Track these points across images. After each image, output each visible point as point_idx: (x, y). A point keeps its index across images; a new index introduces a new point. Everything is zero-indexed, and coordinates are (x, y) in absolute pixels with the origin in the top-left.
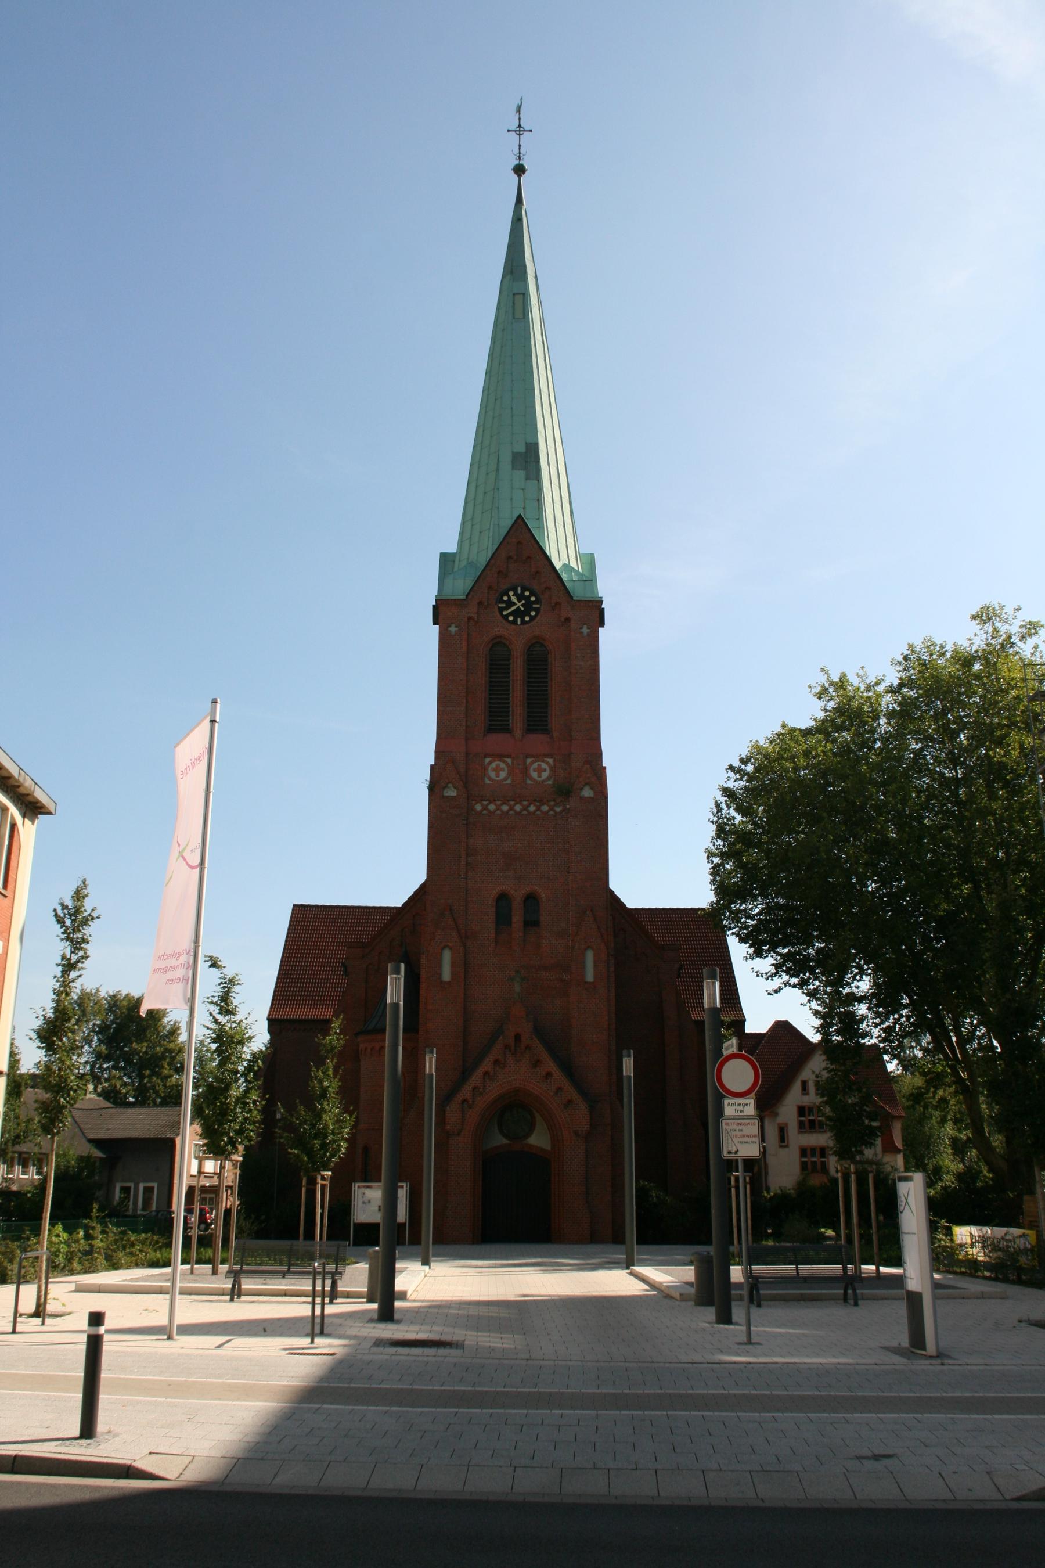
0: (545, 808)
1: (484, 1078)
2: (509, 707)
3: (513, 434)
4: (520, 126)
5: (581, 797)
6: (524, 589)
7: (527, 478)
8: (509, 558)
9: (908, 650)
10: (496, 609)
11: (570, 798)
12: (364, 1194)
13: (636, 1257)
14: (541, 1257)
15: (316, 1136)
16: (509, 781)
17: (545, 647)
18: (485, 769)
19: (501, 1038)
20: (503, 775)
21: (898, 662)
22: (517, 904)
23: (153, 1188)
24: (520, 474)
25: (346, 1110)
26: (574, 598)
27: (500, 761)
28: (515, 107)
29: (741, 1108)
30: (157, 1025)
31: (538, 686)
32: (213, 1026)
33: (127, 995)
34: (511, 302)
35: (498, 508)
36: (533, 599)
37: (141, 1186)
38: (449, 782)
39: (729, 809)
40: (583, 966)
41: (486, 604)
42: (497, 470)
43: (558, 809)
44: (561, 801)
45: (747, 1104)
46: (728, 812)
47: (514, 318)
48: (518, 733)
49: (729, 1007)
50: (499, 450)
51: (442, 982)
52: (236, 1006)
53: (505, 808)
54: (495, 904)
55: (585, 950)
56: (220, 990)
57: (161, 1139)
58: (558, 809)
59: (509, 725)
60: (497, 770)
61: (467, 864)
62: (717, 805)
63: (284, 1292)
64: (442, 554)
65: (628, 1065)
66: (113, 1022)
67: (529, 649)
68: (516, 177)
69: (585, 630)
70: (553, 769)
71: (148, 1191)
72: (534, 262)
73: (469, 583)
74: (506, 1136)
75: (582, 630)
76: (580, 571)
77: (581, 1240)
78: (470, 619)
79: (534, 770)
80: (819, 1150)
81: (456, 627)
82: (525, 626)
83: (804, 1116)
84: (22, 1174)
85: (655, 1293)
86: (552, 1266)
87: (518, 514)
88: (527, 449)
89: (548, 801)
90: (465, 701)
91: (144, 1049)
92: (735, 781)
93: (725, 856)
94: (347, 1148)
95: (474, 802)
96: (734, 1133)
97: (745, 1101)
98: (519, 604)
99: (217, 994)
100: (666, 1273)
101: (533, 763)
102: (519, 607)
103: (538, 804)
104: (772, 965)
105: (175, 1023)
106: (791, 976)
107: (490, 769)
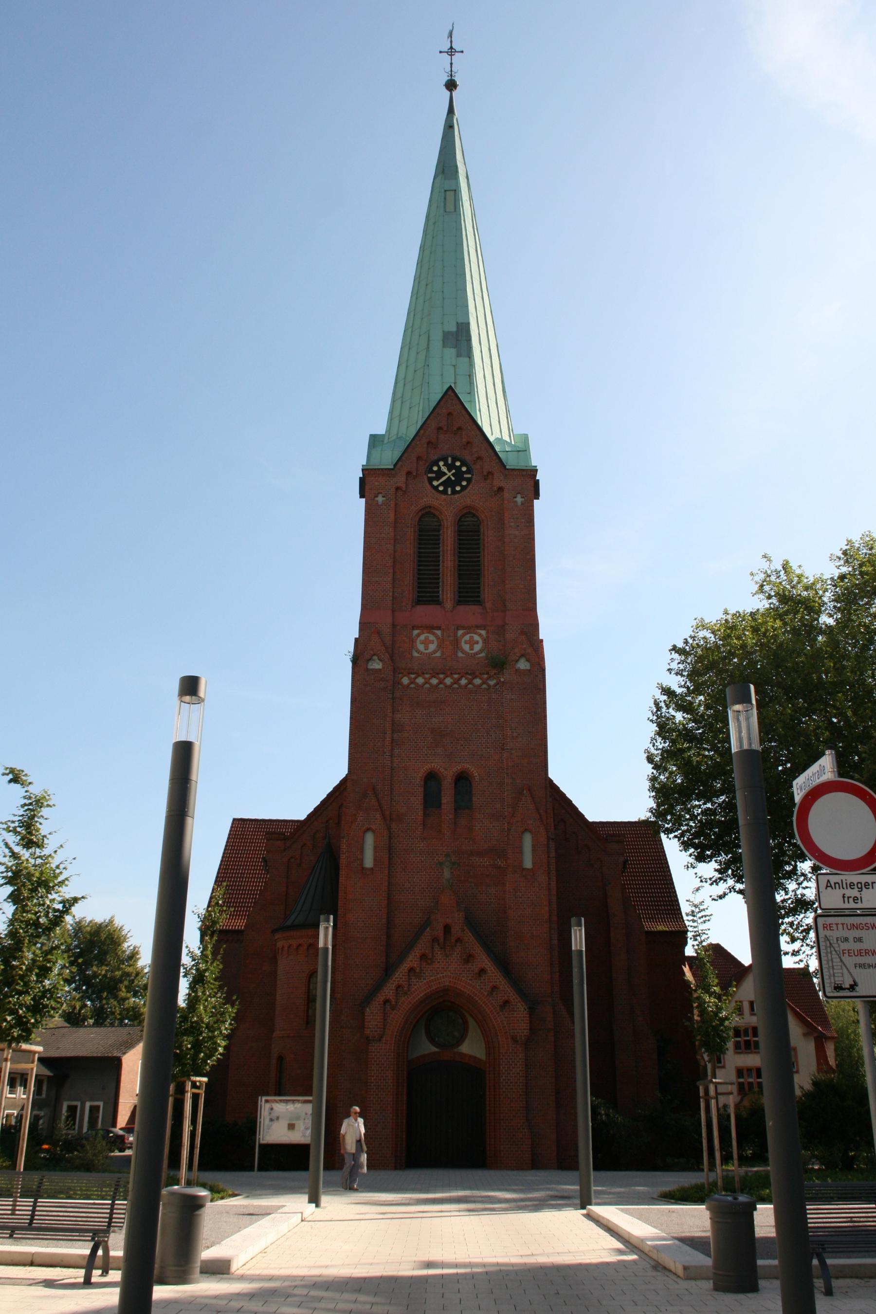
0: (478, 681)
1: (409, 976)
2: (439, 579)
3: (444, 315)
4: (451, 48)
5: (516, 670)
6: (455, 459)
7: (459, 355)
8: (440, 428)
9: (847, 545)
10: (426, 478)
11: (504, 670)
12: (272, 1109)
13: (594, 1188)
14: (471, 1188)
15: (187, 1032)
16: (438, 654)
17: (477, 517)
18: (412, 641)
19: (428, 929)
20: (432, 647)
21: (837, 557)
22: (448, 784)
23: (98, 1107)
24: (451, 352)
25: (228, 1000)
26: (507, 467)
27: (429, 633)
28: (446, 34)
29: (854, 893)
30: (116, 950)
32: (11, 863)
33: (91, 922)
34: (443, 198)
36: (464, 469)
37: (88, 1105)
38: (374, 655)
39: (668, 708)
40: (520, 851)
41: (415, 474)
42: (428, 348)
43: (492, 683)
44: (495, 674)
45: (867, 885)
46: (667, 711)
47: (445, 212)
48: (449, 605)
49: (670, 918)
50: (429, 330)
51: (363, 868)
52: (44, 836)
53: (434, 681)
54: (423, 783)
55: (523, 833)
56: (21, 812)
57: (108, 1057)
58: (492, 683)
59: (438, 596)
60: (426, 643)
61: (393, 741)
62: (657, 704)
63: (29, 1259)
64: (371, 435)
65: (578, 939)
66: (77, 947)
67: (459, 520)
68: (448, 93)
69: (519, 499)
70: (486, 641)
71: (94, 1110)
72: (465, 164)
73: (397, 454)
74: (433, 1041)
75: (515, 499)
76: (513, 443)
77: (520, 1166)
78: (398, 489)
79: (466, 643)
80: (755, 1070)
81: (383, 497)
82: (456, 496)
83: (740, 1037)
84: (9, 1093)
85: (635, 1257)
86: (483, 1202)
87: (448, 386)
88: (458, 328)
89: (481, 674)
90: (392, 571)
91: (103, 972)
92: (679, 663)
93: (667, 755)
94: (225, 1048)
95: (400, 675)
96: (844, 946)
97: (864, 879)
98: (449, 474)
99: (17, 818)
100: (640, 1217)
101: (464, 635)
102: (449, 477)
103: (470, 677)
104: (716, 870)
105: (135, 948)
106: (738, 882)
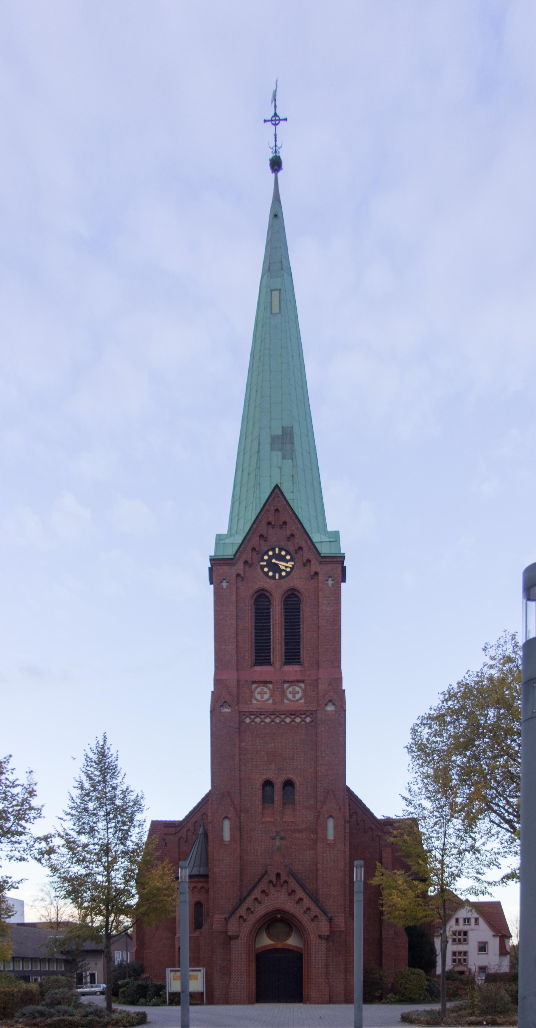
4: (275, 115)
18: (252, 692)
20: (266, 696)
26: (322, 555)
27: (264, 686)
31: (294, 636)
35: (259, 484)
42: (259, 452)
48: (278, 664)
61: (240, 760)
68: (274, 175)
70: (304, 691)
78: (238, 575)
79: (290, 693)
82: (282, 580)
107: (256, 692)
